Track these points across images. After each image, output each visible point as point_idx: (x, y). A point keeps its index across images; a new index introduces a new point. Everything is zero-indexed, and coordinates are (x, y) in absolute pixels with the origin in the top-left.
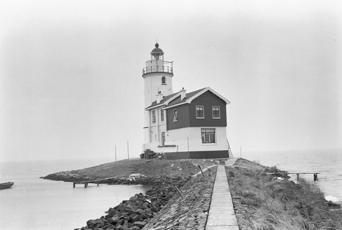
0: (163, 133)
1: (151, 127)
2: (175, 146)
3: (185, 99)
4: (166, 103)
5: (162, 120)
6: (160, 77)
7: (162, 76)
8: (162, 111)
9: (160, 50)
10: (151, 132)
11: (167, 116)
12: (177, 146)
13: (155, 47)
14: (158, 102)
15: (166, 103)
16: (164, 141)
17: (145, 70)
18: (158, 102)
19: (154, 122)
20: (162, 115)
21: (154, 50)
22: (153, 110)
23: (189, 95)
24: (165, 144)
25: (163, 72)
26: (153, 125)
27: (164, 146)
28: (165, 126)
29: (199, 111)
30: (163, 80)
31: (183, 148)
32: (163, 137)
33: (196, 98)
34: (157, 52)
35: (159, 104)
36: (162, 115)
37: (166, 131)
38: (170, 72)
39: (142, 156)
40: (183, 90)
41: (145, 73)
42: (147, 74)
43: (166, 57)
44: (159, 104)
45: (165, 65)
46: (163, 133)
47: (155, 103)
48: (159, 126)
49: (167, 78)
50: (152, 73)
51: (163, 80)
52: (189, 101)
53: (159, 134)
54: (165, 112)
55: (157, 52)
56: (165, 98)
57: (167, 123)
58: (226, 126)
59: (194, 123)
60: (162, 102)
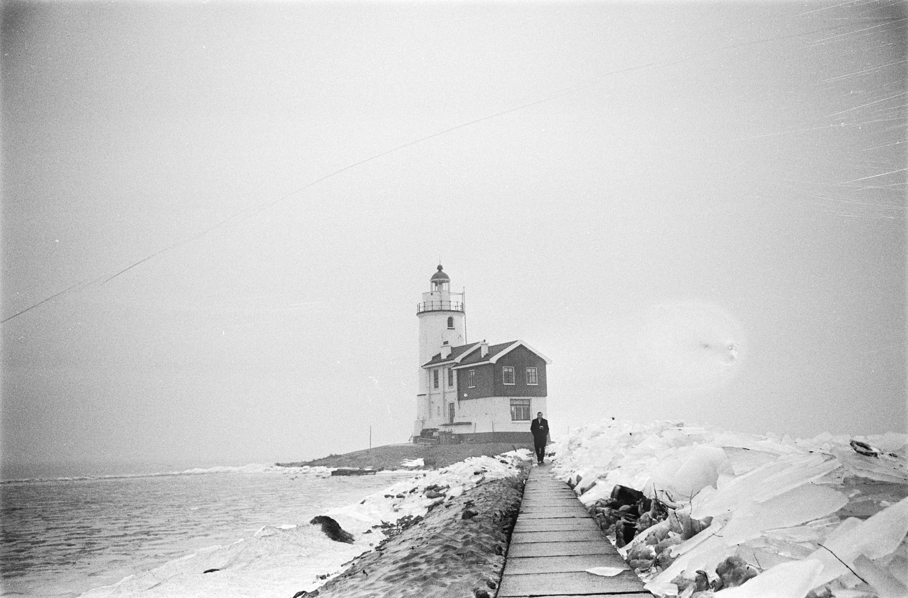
0: (452, 405)
1: (430, 395)
2: (470, 423)
3: (488, 357)
4: (458, 360)
5: (451, 384)
6: (444, 318)
7: (448, 316)
8: (450, 372)
9: (446, 276)
10: (431, 403)
11: (458, 380)
12: (473, 425)
14: (444, 357)
15: (458, 360)
16: (452, 416)
17: (422, 305)
18: (444, 357)
19: (436, 386)
20: (450, 377)
21: (435, 276)
23: (494, 350)
24: (456, 420)
25: (450, 311)
26: (433, 391)
27: (452, 424)
28: (455, 395)
29: (508, 375)
30: (450, 322)
31: (483, 427)
32: (452, 410)
33: (548, 376)
34: (440, 278)
35: (445, 360)
36: (450, 377)
37: (456, 402)
38: (459, 309)
39: (416, 439)
40: (450, 314)
41: (422, 310)
42: (424, 312)
43: (455, 285)
44: (445, 360)
45: (453, 298)
46: (452, 405)
47: (437, 358)
48: (444, 393)
49: (456, 317)
50: (433, 311)
51: (450, 322)
52: (493, 360)
53: (444, 407)
54: (455, 373)
55: (440, 278)
56: (456, 351)
57: (458, 390)
58: (546, 395)
59: (499, 392)
60: (450, 357)
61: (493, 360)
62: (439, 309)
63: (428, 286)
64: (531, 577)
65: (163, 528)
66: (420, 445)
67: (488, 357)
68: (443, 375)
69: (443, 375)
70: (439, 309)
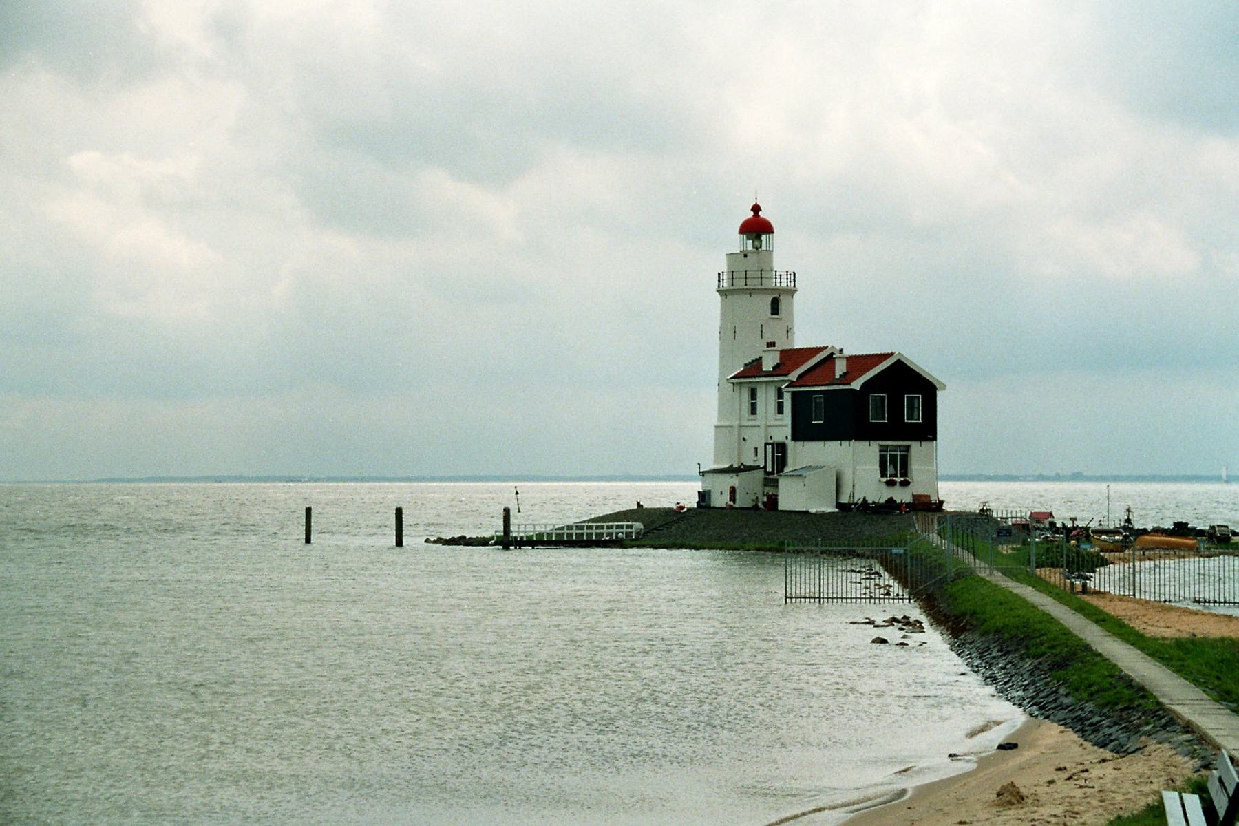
3: (847, 377)
5: (780, 410)
6: (768, 300)
14: (767, 366)
15: (794, 376)
18: (767, 366)
22: (753, 386)
23: (859, 363)
35: (768, 374)
44: (768, 374)
47: (753, 369)
49: (784, 301)
52: (856, 385)
55: (756, 228)
56: (791, 358)
60: (778, 370)
62: (755, 285)
63: (736, 242)
64: (921, 700)
65: (622, 605)
66: (1176, 653)
67: (847, 377)
68: (767, 399)
69: (767, 399)
70: (755, 285)
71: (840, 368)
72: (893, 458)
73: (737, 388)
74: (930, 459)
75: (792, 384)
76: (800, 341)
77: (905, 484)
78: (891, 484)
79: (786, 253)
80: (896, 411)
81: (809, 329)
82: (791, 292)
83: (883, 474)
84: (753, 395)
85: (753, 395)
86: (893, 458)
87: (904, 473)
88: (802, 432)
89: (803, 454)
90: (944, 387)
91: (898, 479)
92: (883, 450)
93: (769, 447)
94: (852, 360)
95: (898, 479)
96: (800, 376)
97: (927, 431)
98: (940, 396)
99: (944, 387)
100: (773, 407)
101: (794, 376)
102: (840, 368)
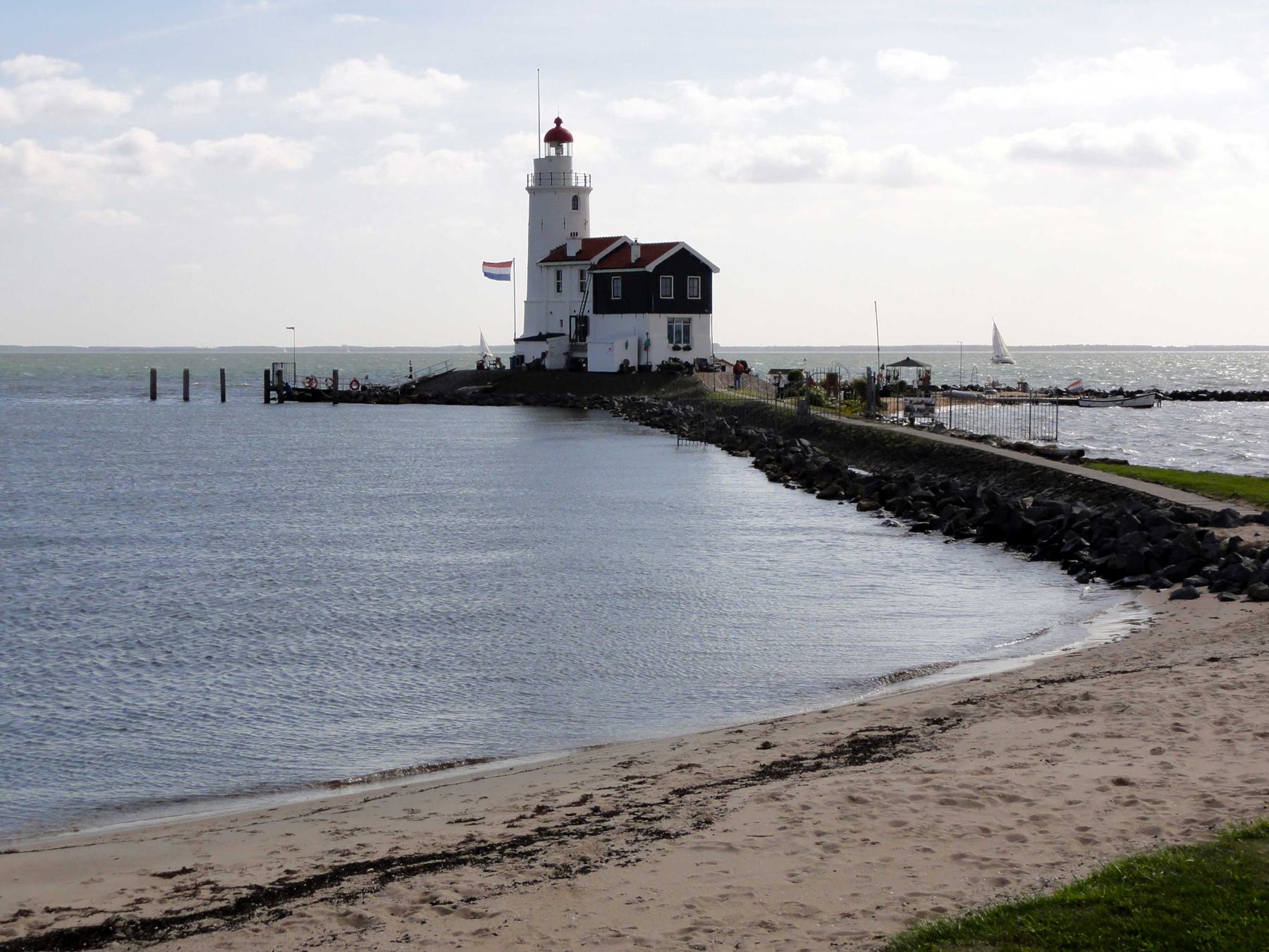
3: (642, 262)
5: (582, 288)
13: (554, 126)
14: (571, 252)
15: (595, 260)
18: (571, 252)
23: (652, 250)
35: (571, 259)
44: (571, 259)
47: (559, 255)
52: (650, 268)
55: (558, 136)
56: (594, 245)
58: (710, 312)
60: (580, 256)
61: (650, 268)
62: (554, 187)
63: (547, 151)
67: (642, 262)
69: (571, 275)
70: (554, 187)
71: (635, 254)
72: (678, 332)
73: (545, 270)
74: (706, 329)
75: (593, 267)
76: (595, 232)
77: (688, 349)
78: (676, 348)
79: (583, 157)
80: (681, 288)
81: (604, 221)
82: (587, 190)
83: (671, 341)
84: (559, 275)
85: (559, 275)
86: (678, 332)
87: (687, 341)
88: (604, 304)
89: (603, 325)
90: (718, 270)
91: (682, 345)
92: (671, 322)
93: (573, 320)
94: (645, 248)
95: (682, 345)
96: (600, 261)
97: (704, 306)
98: (715, 277)
99: (718, 270)
100: (576, 286)
101: (595, 260)
102: (635, 254)
